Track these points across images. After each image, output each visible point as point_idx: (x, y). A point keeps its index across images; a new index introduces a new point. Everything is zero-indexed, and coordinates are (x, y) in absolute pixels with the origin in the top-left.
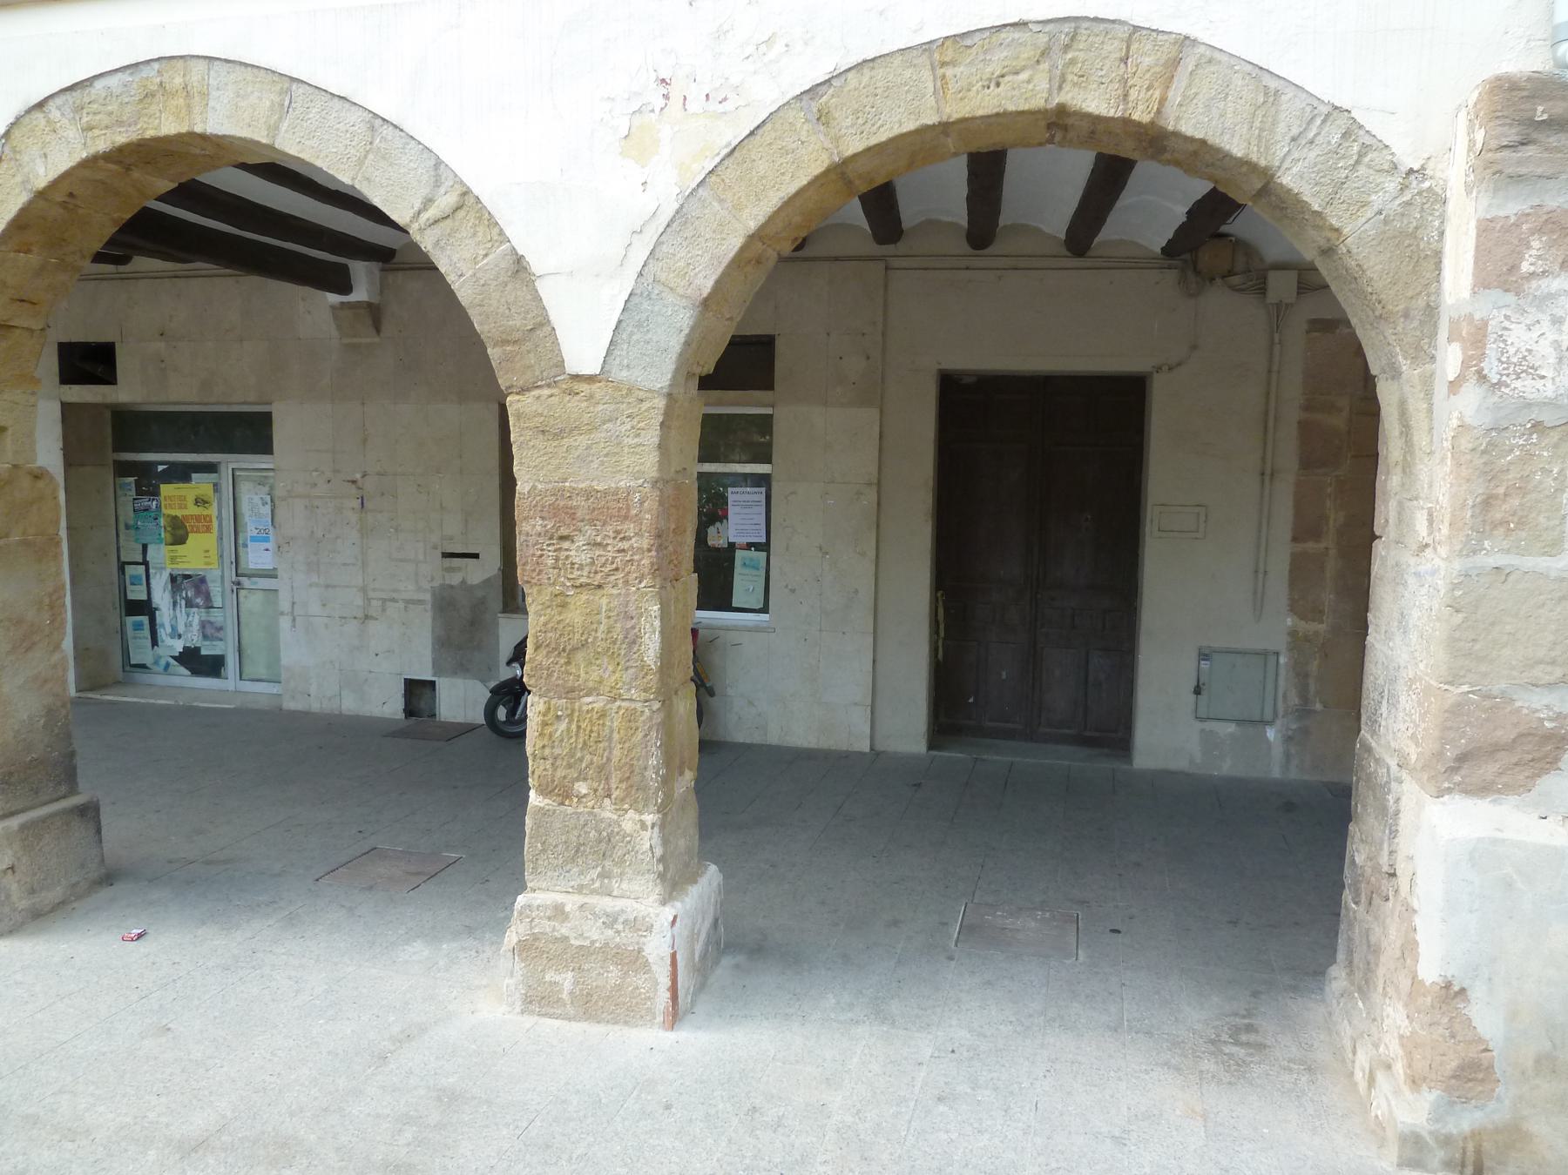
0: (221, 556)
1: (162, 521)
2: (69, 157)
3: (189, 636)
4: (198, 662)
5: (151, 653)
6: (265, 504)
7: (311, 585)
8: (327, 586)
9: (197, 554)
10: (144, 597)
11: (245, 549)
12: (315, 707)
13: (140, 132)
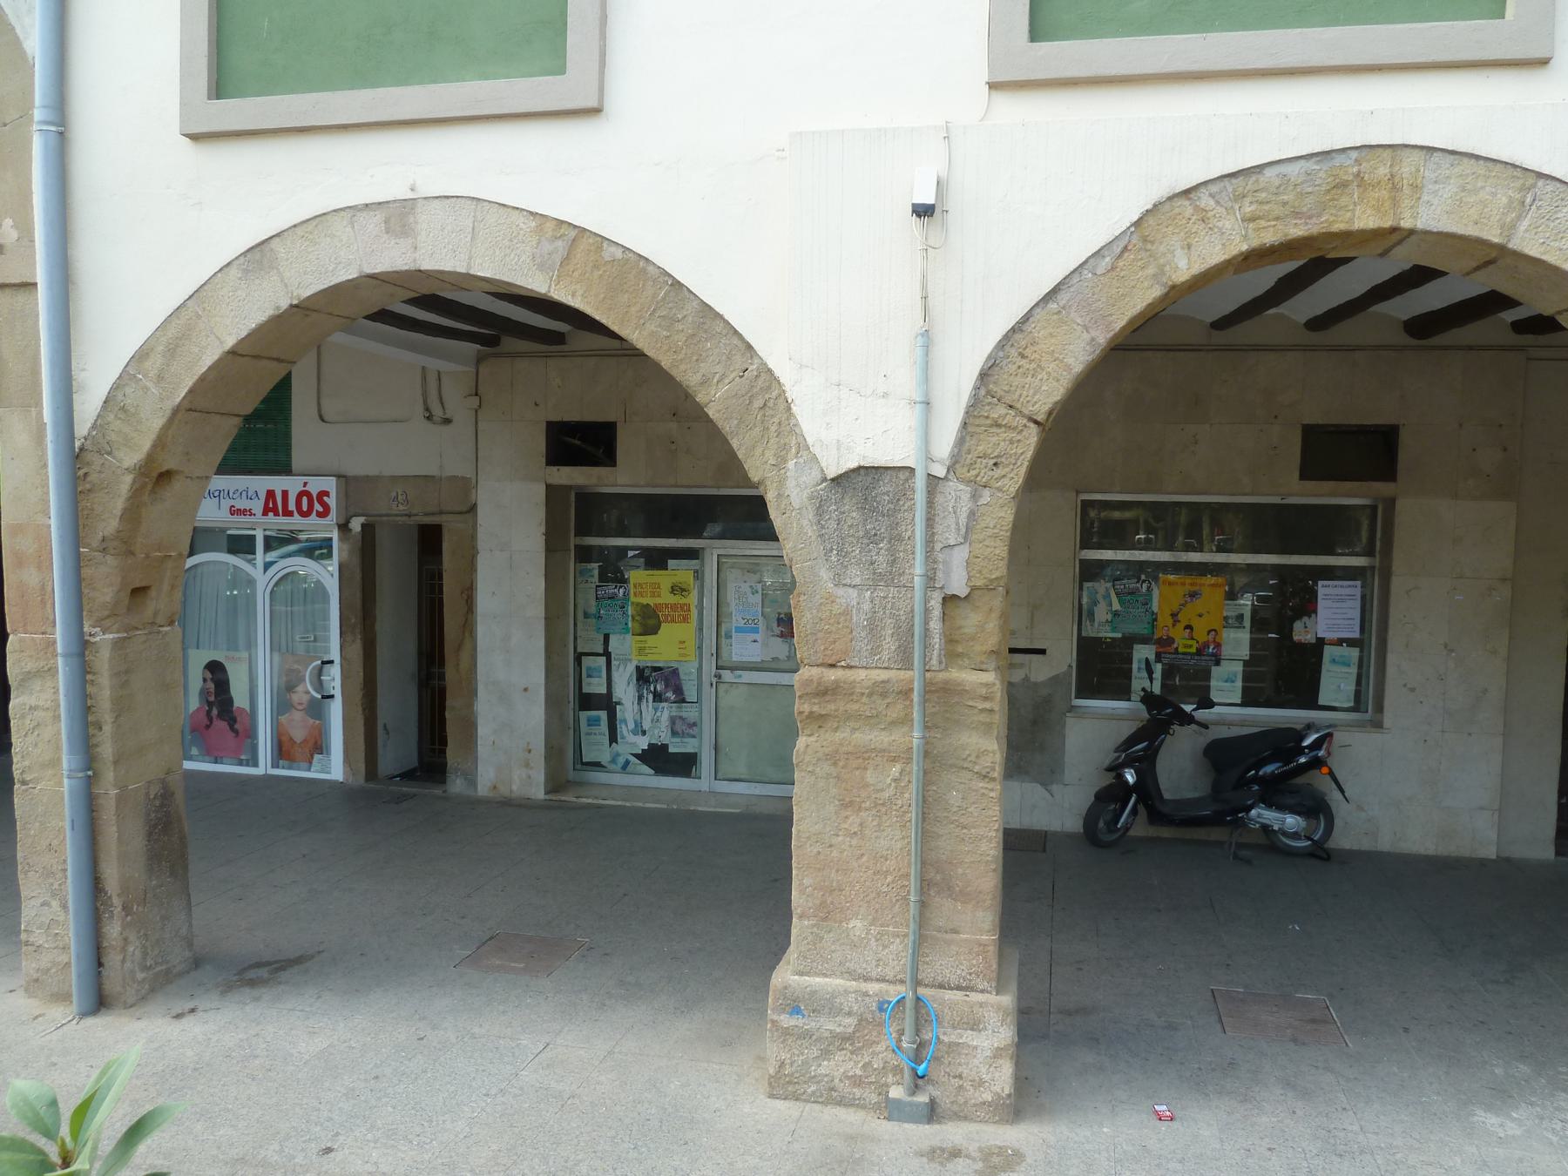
0: (700, 648)
1: (630, 610)
2: (1222, 249)
3: (656, 732)
4: (659, 759)
5: (608, 750)
9: (666, 647)
10: (603, 690)
11: (728, 641)
13: (1325, 225)
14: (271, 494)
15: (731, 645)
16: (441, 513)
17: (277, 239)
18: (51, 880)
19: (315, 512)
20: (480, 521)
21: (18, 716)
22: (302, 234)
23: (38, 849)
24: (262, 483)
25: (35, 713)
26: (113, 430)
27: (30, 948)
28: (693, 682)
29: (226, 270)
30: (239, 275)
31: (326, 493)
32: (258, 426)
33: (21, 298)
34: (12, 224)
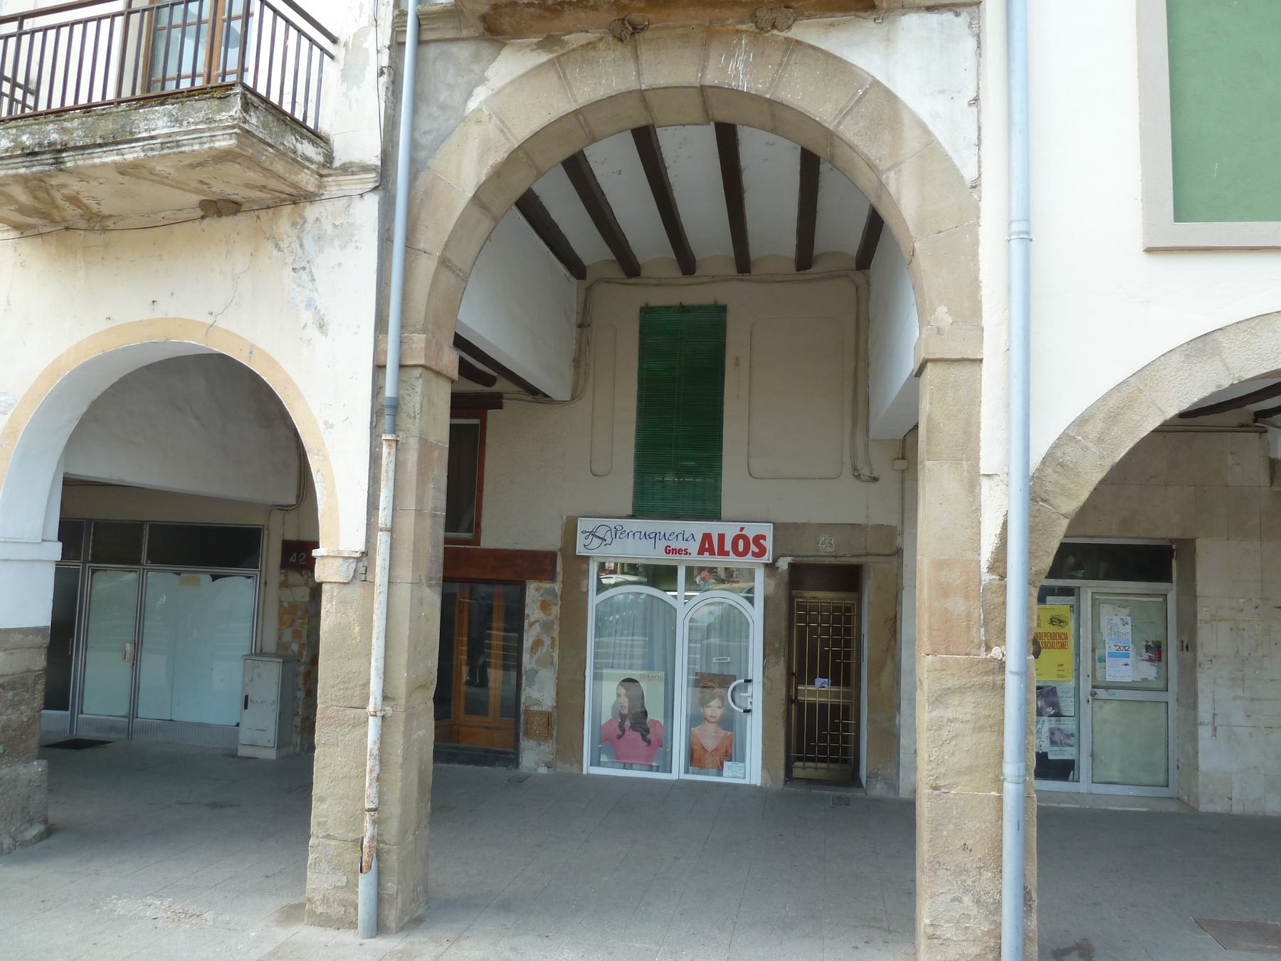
6: (1125, 624)
7: (1234, 699)
8: (1252, 700)
11: (1102, 664)
12: (1237, 809)
14: (707, 537)
15: (1105, 668)
16: (867, 555)
17: (1220, 332)
18: (964, 877)
19: (750, 553)
20: (905, 562)
21: (934, 728)
22: (1245, 329)
23: (950, 848)
24: (698, 528)
25: (953, 724)
26: (1050, 482)
27: (935, 941)
28: (1070, 699)
29: (1168, 355)
30: (1182, 359)
31: (764, 538)
32: (697, 480)
33: (976, 366)
34: (947, 311)
